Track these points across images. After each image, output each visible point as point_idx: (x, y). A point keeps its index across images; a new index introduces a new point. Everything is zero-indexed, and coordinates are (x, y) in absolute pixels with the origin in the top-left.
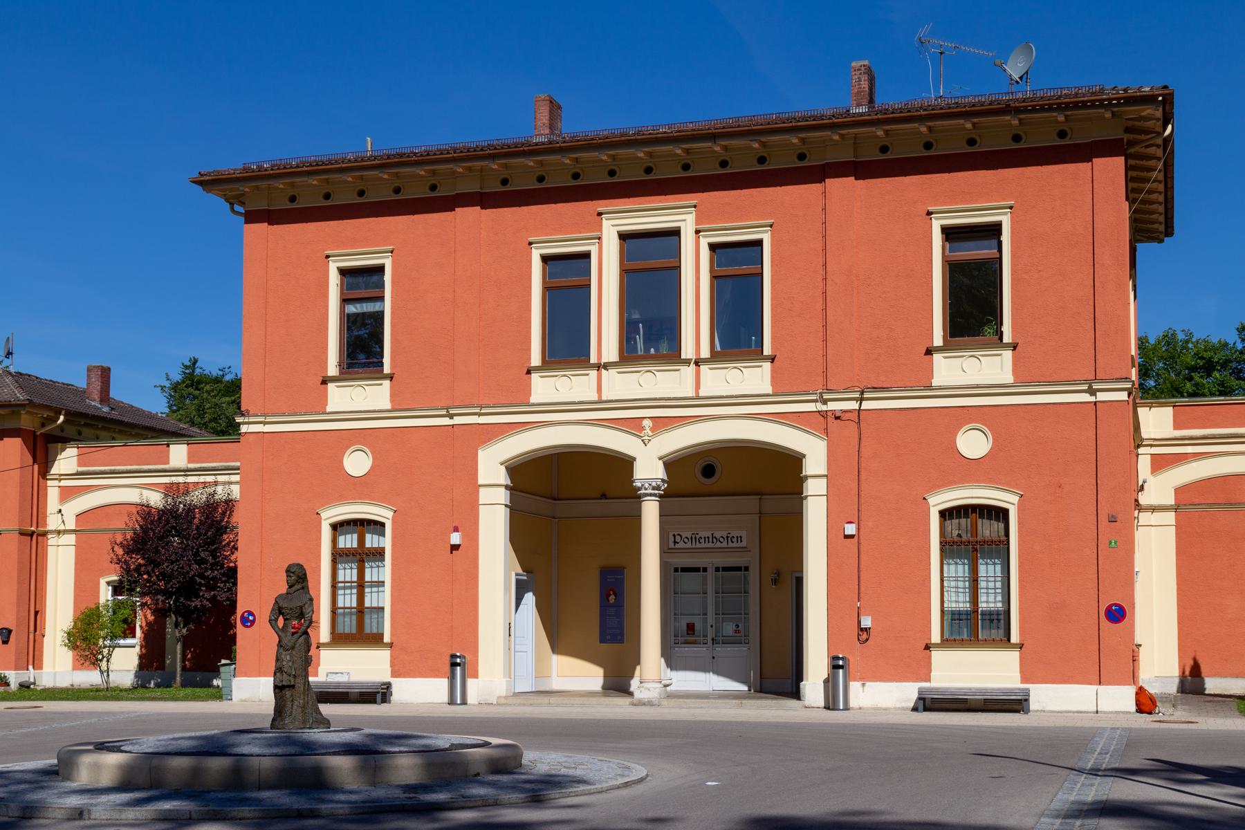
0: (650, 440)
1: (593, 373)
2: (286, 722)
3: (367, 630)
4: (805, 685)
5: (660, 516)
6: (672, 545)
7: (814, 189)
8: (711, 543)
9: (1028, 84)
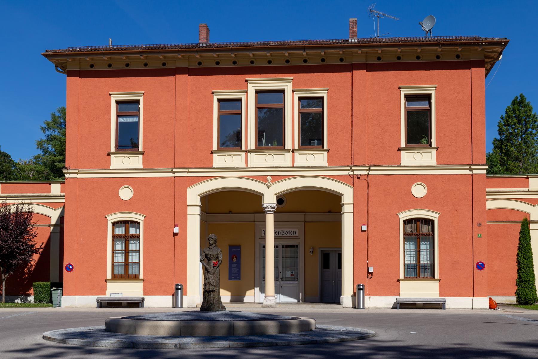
0: (271, 186)
1: (243, 155)
2: (211, 307)
3: (130, 273)
4: (343, 298)
7: (171, 78)
8: (281, 234)
9: (431, 33)
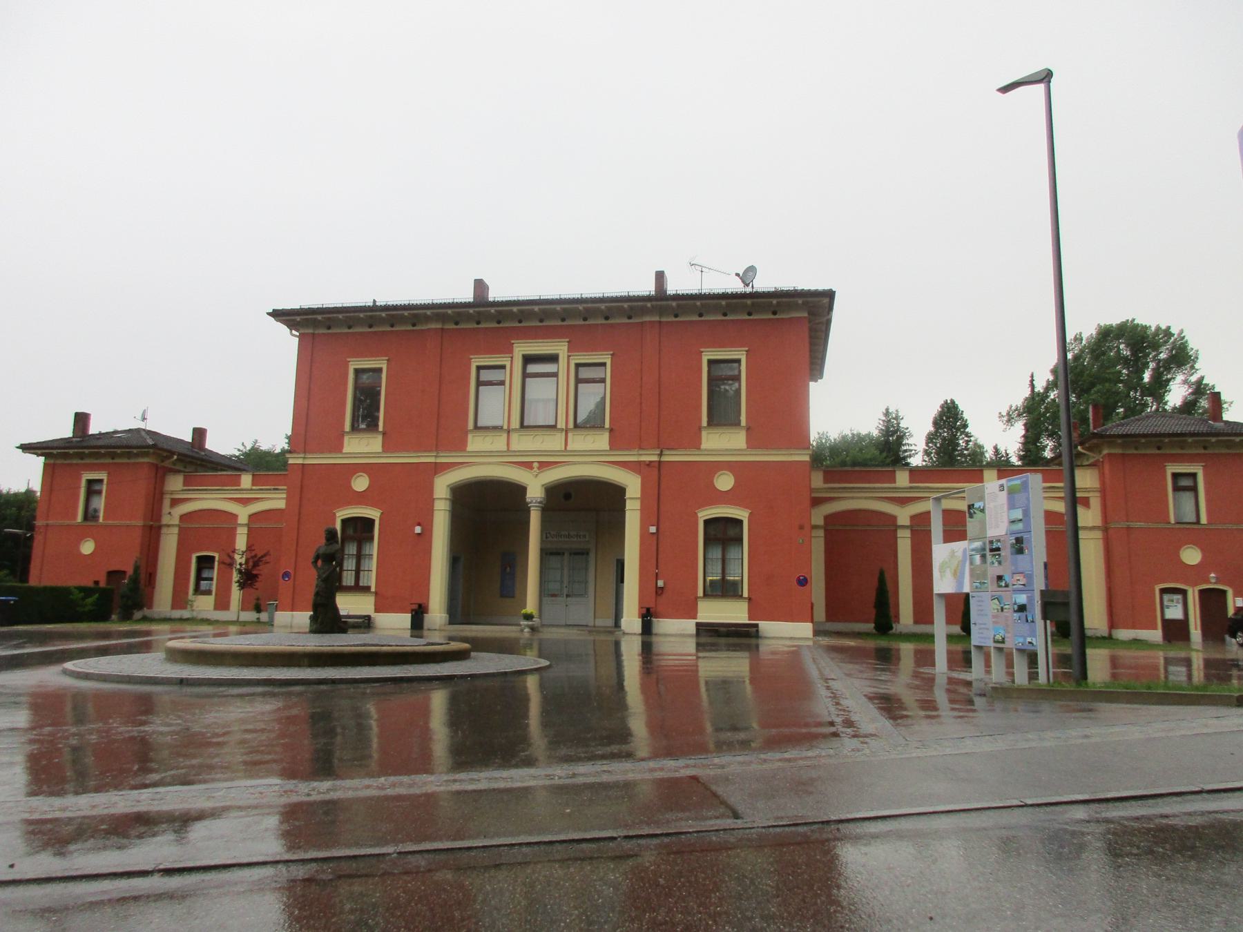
3: (361, 584)
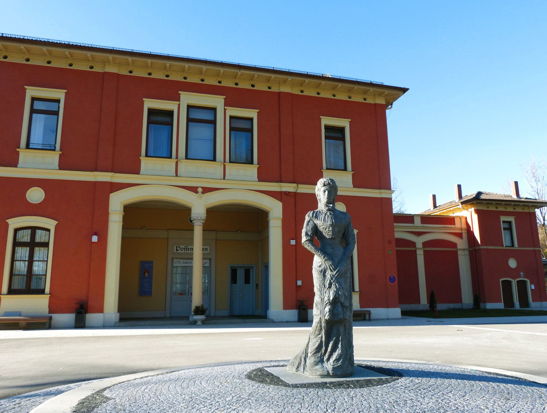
5: (203, 230)
6: (175, 251)
